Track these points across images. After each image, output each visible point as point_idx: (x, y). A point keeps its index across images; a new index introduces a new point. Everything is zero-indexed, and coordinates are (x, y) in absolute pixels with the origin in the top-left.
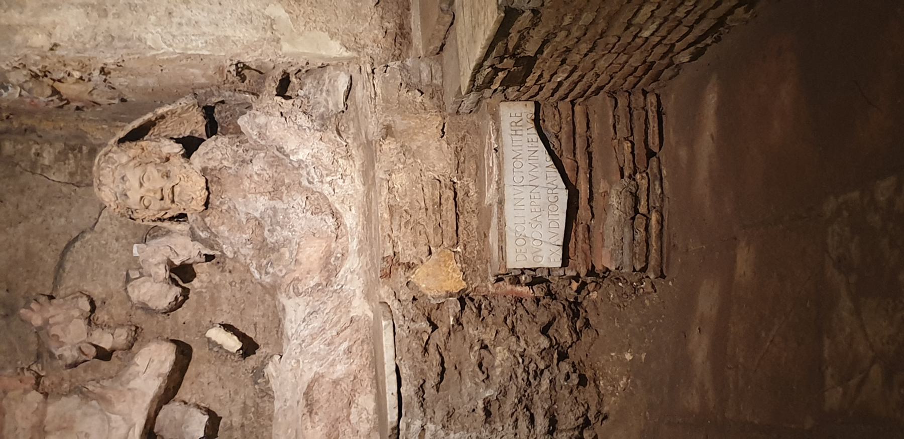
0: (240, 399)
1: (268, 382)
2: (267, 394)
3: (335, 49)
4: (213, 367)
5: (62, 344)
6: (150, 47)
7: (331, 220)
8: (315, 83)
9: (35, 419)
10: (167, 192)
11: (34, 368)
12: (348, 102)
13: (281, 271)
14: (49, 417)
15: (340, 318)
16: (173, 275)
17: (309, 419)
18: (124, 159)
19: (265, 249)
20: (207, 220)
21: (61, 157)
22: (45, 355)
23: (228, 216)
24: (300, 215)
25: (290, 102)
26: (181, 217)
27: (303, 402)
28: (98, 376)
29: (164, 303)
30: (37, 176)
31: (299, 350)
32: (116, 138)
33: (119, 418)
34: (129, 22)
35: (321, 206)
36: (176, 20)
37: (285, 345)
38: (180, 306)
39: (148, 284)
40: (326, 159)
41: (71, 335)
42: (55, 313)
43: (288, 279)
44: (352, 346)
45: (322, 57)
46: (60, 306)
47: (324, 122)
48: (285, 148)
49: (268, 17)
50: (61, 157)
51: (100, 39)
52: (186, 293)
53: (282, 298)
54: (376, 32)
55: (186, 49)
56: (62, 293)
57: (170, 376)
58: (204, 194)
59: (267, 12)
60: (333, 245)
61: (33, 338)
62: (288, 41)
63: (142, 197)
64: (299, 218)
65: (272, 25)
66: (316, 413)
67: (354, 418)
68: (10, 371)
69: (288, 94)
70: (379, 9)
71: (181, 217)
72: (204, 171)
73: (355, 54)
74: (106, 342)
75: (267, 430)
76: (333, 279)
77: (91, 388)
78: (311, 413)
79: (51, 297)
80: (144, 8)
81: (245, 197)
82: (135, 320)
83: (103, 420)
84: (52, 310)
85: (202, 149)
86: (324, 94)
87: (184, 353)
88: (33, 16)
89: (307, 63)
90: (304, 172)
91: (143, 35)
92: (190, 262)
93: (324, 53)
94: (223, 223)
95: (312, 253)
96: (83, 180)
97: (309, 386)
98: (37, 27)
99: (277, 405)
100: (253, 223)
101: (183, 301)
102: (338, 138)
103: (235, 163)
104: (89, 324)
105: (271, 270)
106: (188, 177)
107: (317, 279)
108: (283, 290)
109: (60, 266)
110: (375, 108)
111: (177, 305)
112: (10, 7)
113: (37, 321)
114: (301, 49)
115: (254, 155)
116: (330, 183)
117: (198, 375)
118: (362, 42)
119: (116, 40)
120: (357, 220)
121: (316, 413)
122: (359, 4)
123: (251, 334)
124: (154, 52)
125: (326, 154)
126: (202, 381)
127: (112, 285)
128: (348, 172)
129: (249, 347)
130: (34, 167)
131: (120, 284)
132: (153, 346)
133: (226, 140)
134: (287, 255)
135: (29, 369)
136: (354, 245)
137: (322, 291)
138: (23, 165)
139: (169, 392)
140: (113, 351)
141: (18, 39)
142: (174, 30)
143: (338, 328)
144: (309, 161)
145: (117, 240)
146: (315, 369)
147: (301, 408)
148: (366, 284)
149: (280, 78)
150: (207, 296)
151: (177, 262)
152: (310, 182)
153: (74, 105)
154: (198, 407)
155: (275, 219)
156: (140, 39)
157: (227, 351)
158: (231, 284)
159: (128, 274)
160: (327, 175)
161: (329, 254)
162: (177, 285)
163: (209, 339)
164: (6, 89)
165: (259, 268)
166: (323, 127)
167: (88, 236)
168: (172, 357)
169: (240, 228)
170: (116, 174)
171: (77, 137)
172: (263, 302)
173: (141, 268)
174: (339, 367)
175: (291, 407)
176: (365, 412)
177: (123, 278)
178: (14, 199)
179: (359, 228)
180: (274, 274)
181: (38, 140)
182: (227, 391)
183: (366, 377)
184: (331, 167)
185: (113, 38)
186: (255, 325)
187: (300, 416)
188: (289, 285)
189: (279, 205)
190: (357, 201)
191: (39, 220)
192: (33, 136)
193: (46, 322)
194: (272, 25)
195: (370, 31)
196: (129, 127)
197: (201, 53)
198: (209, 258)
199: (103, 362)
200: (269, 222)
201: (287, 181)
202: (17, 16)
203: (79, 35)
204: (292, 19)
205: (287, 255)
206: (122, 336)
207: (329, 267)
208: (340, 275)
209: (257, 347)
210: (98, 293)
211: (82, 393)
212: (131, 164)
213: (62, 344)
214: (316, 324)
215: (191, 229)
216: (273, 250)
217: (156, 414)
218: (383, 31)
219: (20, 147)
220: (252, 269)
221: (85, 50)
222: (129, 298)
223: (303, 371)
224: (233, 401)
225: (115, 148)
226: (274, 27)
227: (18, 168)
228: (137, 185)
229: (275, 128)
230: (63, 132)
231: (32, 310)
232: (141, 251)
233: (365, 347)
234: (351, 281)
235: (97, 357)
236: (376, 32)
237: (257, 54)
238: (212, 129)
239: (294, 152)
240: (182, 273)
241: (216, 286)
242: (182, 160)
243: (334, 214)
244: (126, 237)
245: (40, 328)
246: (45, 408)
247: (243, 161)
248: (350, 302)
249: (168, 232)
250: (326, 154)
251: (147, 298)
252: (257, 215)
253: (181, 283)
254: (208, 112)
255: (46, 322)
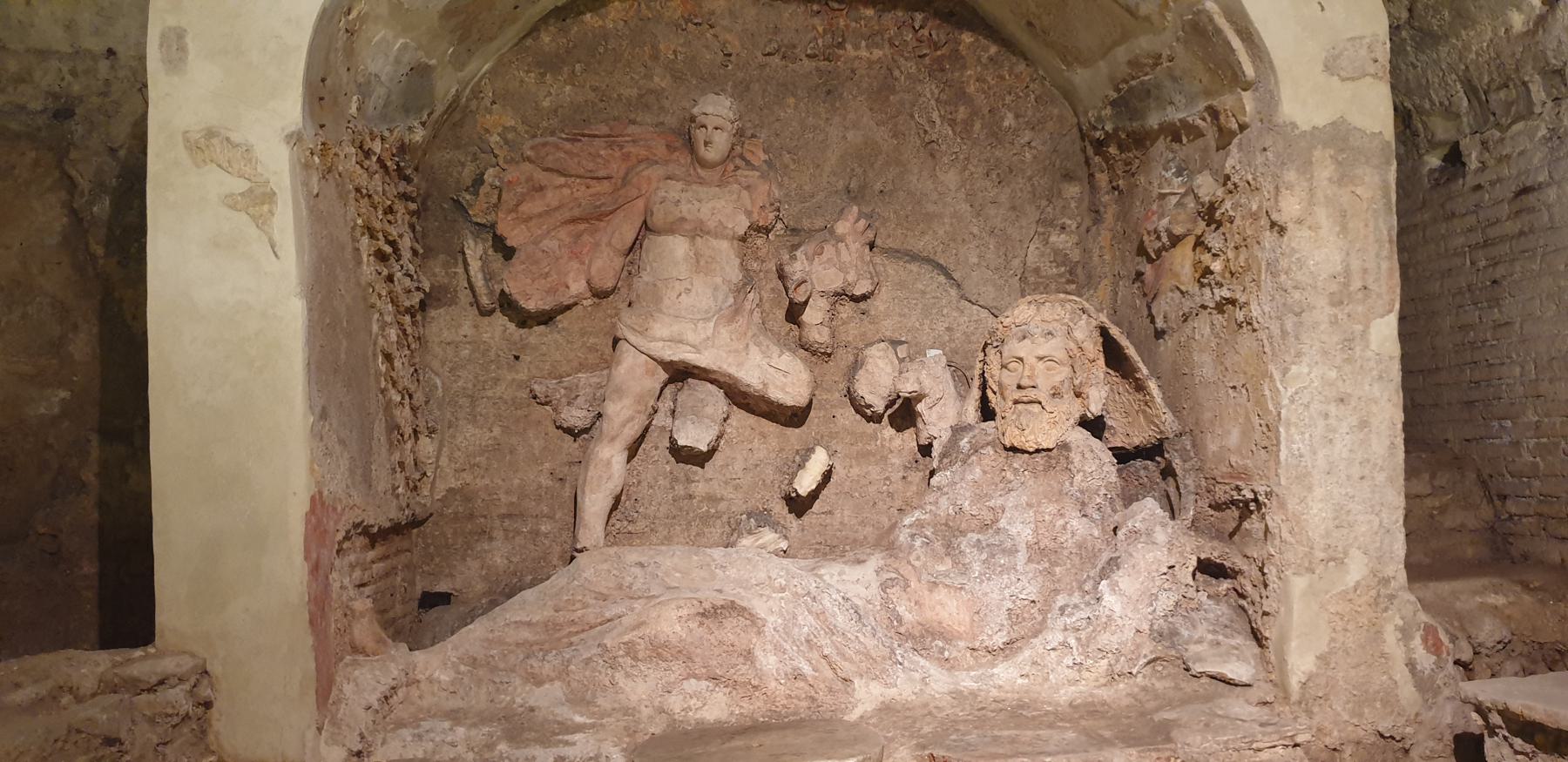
0: (728, 492)
1: (750, 533)
2: (732, 535)
3: (1301, 664)
4: (773, 455)
5: (810, 259)
6: (1285, 372)
7: (1001, 641)
8: (1223, 620)
9: (711, 224)
10: (1032, 394)
11: (779, 225)
12: (1204, 680)
13: (918, 559)
14: (714, 242)
15: (850, 660)
16: (899, 402)
17: (693, 611)
18: (1079, 335)
19: (949, 534)
20: (990, 450)
21: (1060, 257)
22: (796, 240)
23: (997, 480)
24: (1007, 592)
25: (1190, 580)
26: (987, 413)
27: (719, 600)
28: (767, 306)
29: (863, 390)
30: (1034, 226)
31: (799, 590)
32: (1108, 324)
33: (709, 332)
34: (1324, 337)
35: (1025, 628)
36: (1333, 409)
37: (803, 563)
38: (857, 411)
39: (889, 369)
40: (1106, 639)
41: (823, 270)
42: (852, 251)
43: (906, 570)
44: (805, 679)
45: (1283, 639)
46: (862, 257)
47: (1166, 636)
48: (1120, 573)
49: (1346, 554)
50: (1060, 257)
51: (1297, 295)
52: (875, 418)
53: (876, 561)
54: (1335, 733)
55: (1288, 425)
56: (877, 260)
57: (764, 399)
58: (1031, 447)
59: (1355, 553)
60: (962, 644)
61: (819, 223)
62: (1310, 586)
63: (1021, 359)
64: (1002, 590)
65: (1334, 559)
66: (701, 624)
67: (692, 685)
68: (777, 193)
69: (1198, 575)
70: (1373, 739)
71: (987, 413)
72: (1064, 446)
73: (1295, 697)
74: (811, 316)
75: (683, 531)
76: (909, 644)
77: (751, 296)
78: (703, 615)
79: (872, 246)
80: (1348, 361)
81: (1030, 505)
82: (841, 351)
83: (707, 312)
84: (854, 246)
85: (1095, 442)
86: (1210, 637)
87: (794, 417)
88: (1326, 197)
89: (1265, 614)
90: (1076, 599)
91: (1306, 359)
92: (920, 425)
93: (1293, 644)
94: (985, 472)
95: (949, 609)
96: (1030, 284)
97: (744, 609)
98: (1311, 202)
99: (718, 553)
100: (988, 517)
101: (864, 415)
102: (1143, 661)
103: (1082, 492)
104: (837, 294)
105: (918, 543)
106: (1055, 423)
107: (908, 617)
108: (889, 561)
109: (914, 257)
110: (1235, 750)
111: (860, 408)
112: (1340, 163)
113: (842, 228)
114: (1297, 606)
115: (1093, 521)
116: (1065, 644)
117: (763, 436)
118: (1316, 709)
119: (1296, 319)
120: (1008, 688)
121: (701, 624)
122: (1378, 705)
123: (817, 506)
124: (1277, 376)
125: (1115, 639)
126: (756, 443)
127: (887, 323)
128: (1086, 674)
129: (799, 505)
130: (1047, 223)
131: (888, 334)
132: (805, 376)
133: (1114, 478)
134: (942, 568)
135: (777, 217)
136: (967, 682)
137: (890, 627)
138: (1049, 209)
139: (741, 398)
140: (799, 324)
141: (1291, 176)
142: (1315, 406)
143: (835, 658)
144: (1102, 612)
145: (948, 329)
146: (771, 619)
147: (711, 597)
148: (907, 707)
149: (1227, 564)
150: (871, 447)
151: (920, 407)
152: (1062, 609)
153: (1148, 269)
154: (719, 437)
155: (998, 551)
156: (1299, 354)
157: (794, 475)
158: (887, 478)
159: (902, 343)
160: (1078, 639)
161: (948, 637)
162: (887, 407)
163: (811, 450)
164: (1179, 174)
165: (920, 524)
166: (1158, 636)
167: (953, 292)
168: (789, 401)
169: (979, 498)
170: (1055, 324)
171: (1090, 277)
172: (862, 523)
173: (911, 360)
174: (772, 659)
175: (713, 577)
176: (699, 704)
177: (896, 336)
178: (1003, 198)
179: (994, 693)
180: (911, 547)
181: (1083, 228)
182: (740, 475)
183: (754, 707)
184: (1093, 647)
185: (1298, 314)
186: (830, 512)
187: (699, 595)
188: (897, 571)
189: (1022, 557)
190: (1038, 688)
191: (975, 230)
192: (1088, 222)
193: (841, 239)
194: (1334, 559)
195: (1336, 723)
196: (1124, 342)
197: (1283, 447)
198: (926, 450)
199: (783, 312)
200: (991, 541)
201: (1058, 569)
202: (1326, 174)
203: (1301, 264)
204: (1346, 592)
205: (942, 568)
206: (818, 335)
207: (925, 638)
208: (917, 658)
209: (799, 515)
210: (878, 305)
211: (745, 285)
212: (1072, 345)
213: (810, 259)
214: (841, 620)
215: (969, 428)
216: (948, 546)
217: (712, 382)
218: (1337, 745)
219: (1073, 205)
220: (917, 514)
221: (1274, 275)
222: (872, 344)
223: (769, 597)
224: (726, 483)
225: (1094, 323)
226: (1332, 564)
227: (1044, 203)
228: (1041, 353)
229: (1150, 557)
230: (1096, 258)
231: (857, 221)
232: (936, 360)
233: (804, 704)
234: (911, 680)
235: (791, 303)
236: (1335, 733)
237: (1285, 535)
238: (1123, 456)
239: (1114, 588)
240: (904, 413)
241: (884, 459)
242: (1077, 416)
243: (1010, 648)
244: (951, 340)
245: (832, 232)
246: (724, 237)
247: (1083, 504)
248: (876, 678)
249: (962, 397)
250: (1115, 639)
251: (869, 367)
252: (1002, 523)
253: (890, 411)
254: (1152, 451)
255: (841, 239)
